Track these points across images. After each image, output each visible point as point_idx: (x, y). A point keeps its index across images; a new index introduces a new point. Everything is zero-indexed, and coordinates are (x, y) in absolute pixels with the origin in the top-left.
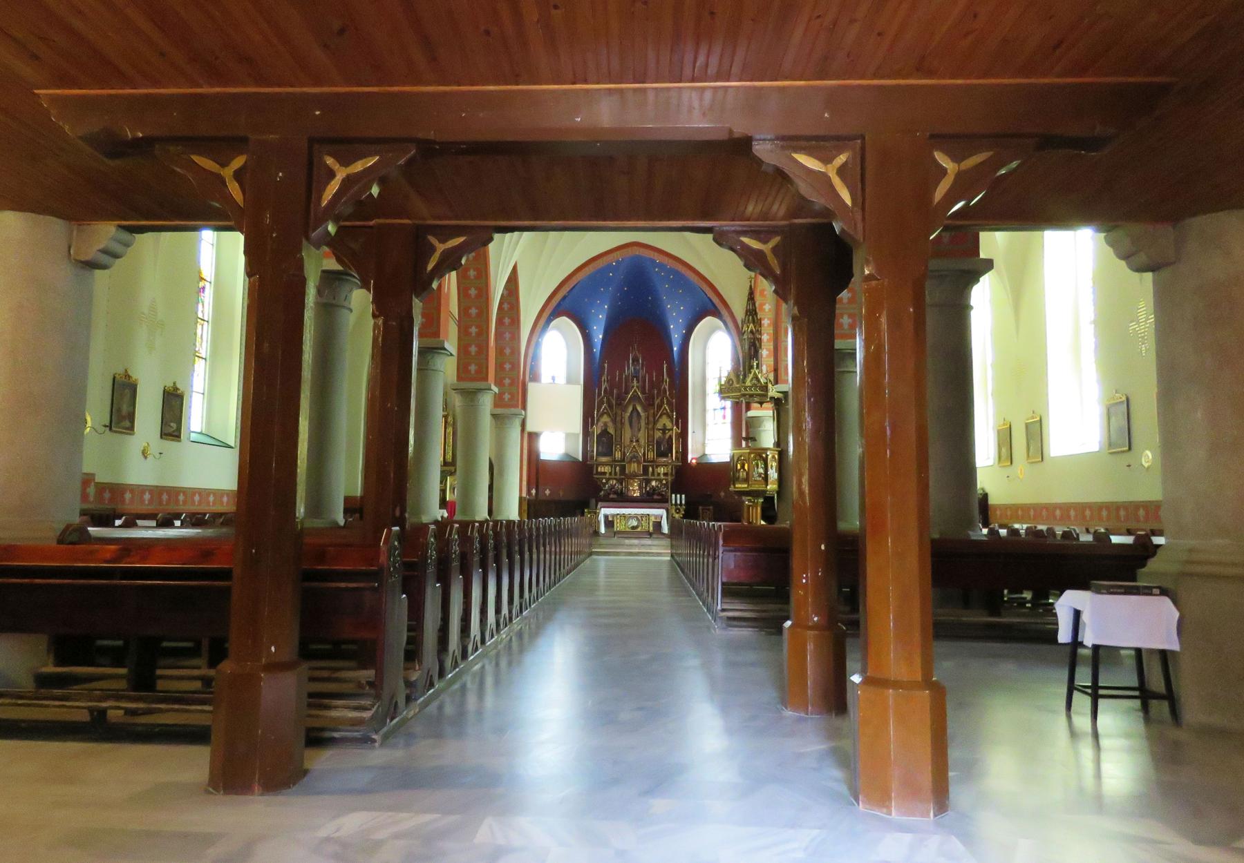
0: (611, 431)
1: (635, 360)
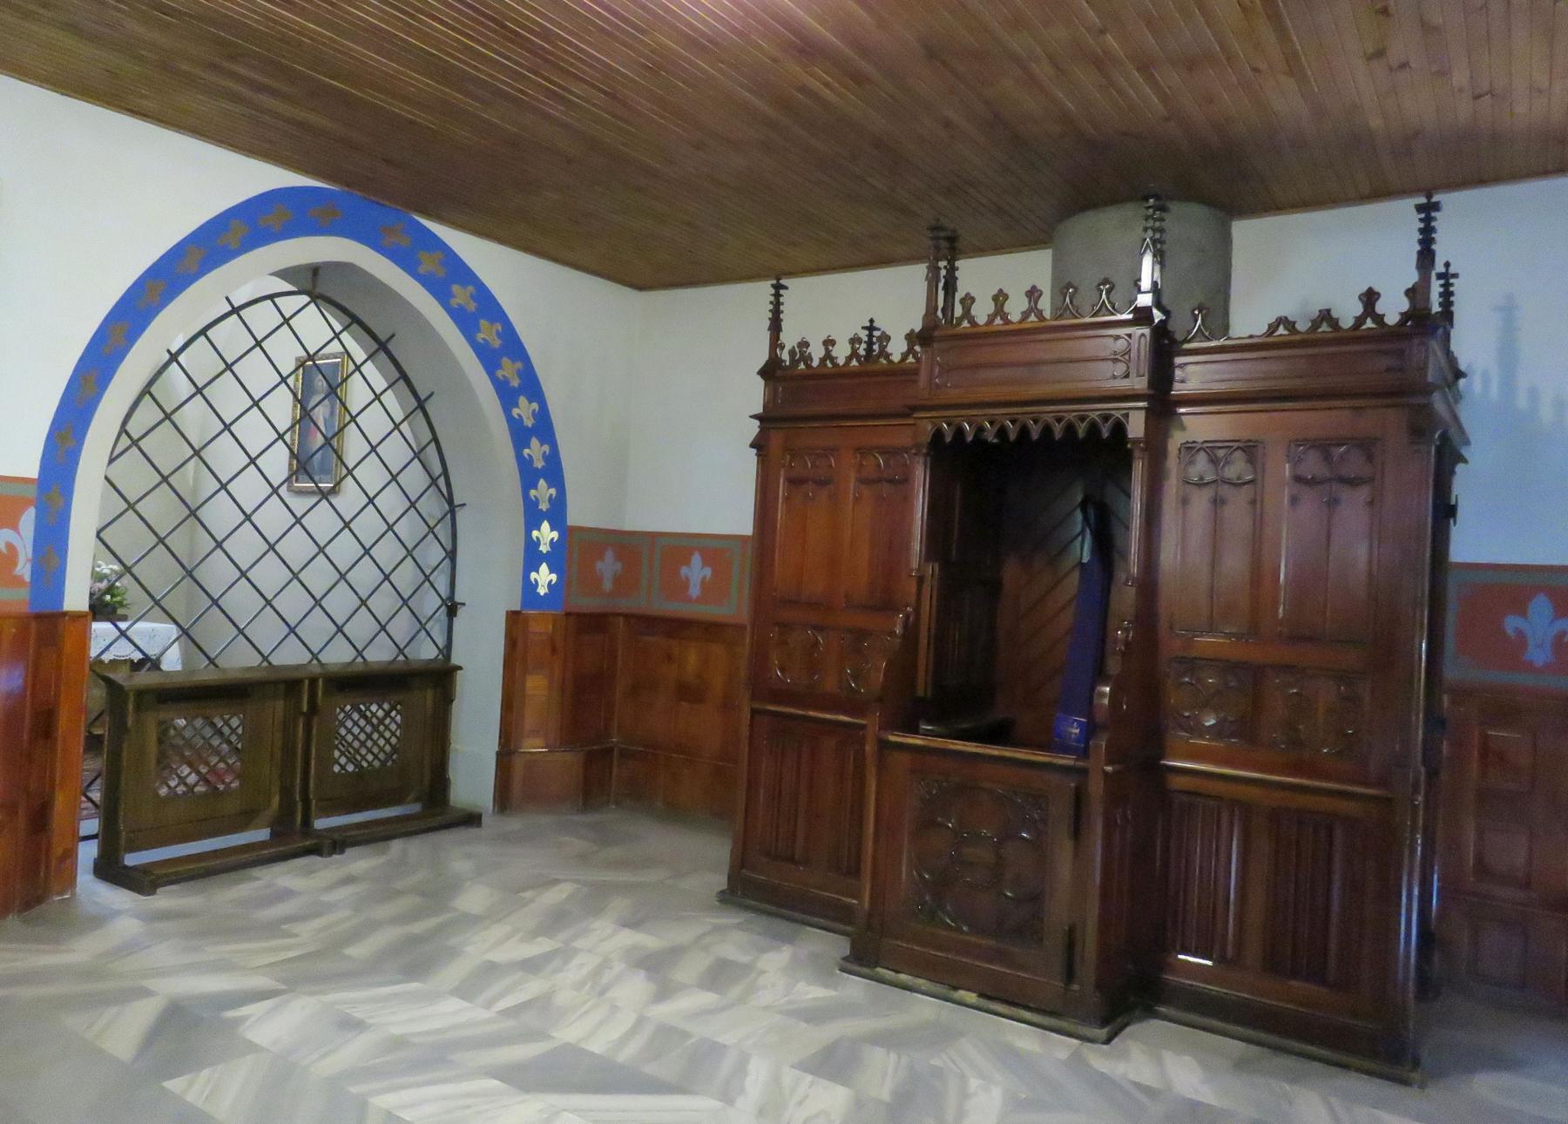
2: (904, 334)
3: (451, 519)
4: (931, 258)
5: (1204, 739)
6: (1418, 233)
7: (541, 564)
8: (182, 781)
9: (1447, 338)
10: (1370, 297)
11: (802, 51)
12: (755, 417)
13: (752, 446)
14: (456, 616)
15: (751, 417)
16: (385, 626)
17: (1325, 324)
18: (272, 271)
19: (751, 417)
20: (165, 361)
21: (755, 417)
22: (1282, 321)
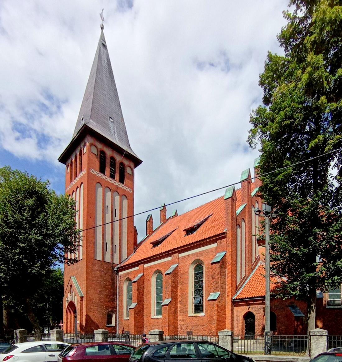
15: (18, 347)
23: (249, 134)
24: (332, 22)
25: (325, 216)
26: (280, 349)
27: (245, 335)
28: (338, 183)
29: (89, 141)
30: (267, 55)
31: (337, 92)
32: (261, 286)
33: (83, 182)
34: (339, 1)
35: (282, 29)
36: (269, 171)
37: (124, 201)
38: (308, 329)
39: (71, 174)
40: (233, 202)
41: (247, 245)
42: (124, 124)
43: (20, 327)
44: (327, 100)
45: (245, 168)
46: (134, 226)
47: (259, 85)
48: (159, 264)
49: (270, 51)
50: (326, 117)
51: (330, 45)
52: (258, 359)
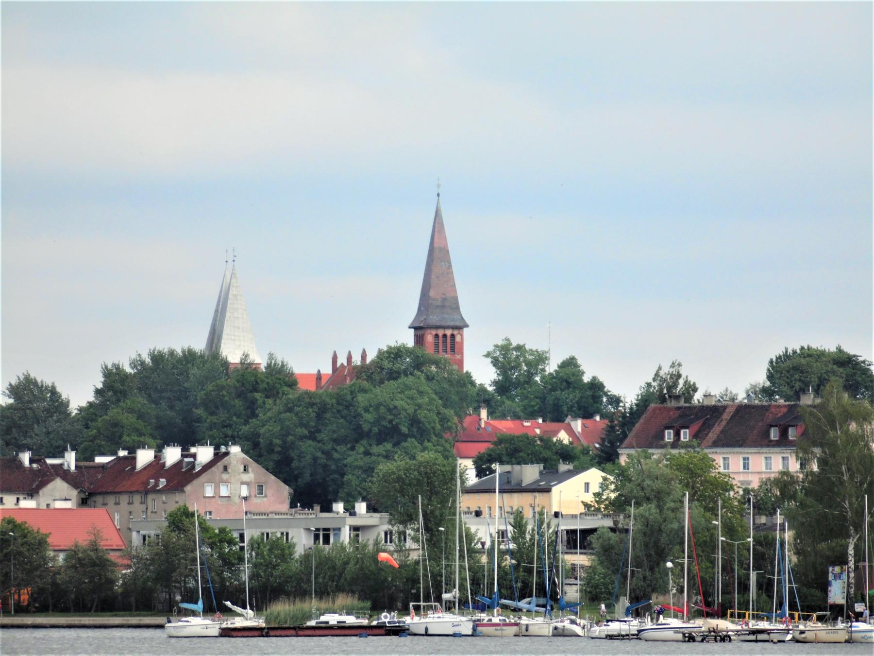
0: (856, 521)
1: (549, 526)
2: (776, 351)
3: (336, 362)
4: (605, 399)
5: (486, 475)
6: (93, 394)
7: (370, 363)
8: (618, 431)
9: (231, 363)
10: (468, 474)
11: (377, 540)
12: (319, 371)
13: (183, 491)
14: (564, 361)
15: (583, 502)
16: (371, 423)
17: (712, 503)
18: (337, 353)
19: (583, 502)
20: (224, 342)
21: (319, 371)
22: (130, 364)
23: (717, 396)
24: (134, 552)
25: (699, 606)
26: (459, 613)
27: (455, 614)
28: (157, 349)
29: (424, 633)
30: (296, 547)
31: (130, 467)
32: (410, 474)
33: (491, 506)
34: (871, 375)
35: (26, 523)
36: (725, 548)
37: (413, 345)
38: (458, 505)
39: (363, 631)
40: (87, 441)
41: (222, 298)
42: (313, 651)
43: (294, 487)
44: (91, 404)
45: (766, 368)
46: (341, 541)
47: (840, 347)
48: (494, 584)
49: (485, 353)
50: (277, 454)
51: (564, 437)
52: (455, 624)
